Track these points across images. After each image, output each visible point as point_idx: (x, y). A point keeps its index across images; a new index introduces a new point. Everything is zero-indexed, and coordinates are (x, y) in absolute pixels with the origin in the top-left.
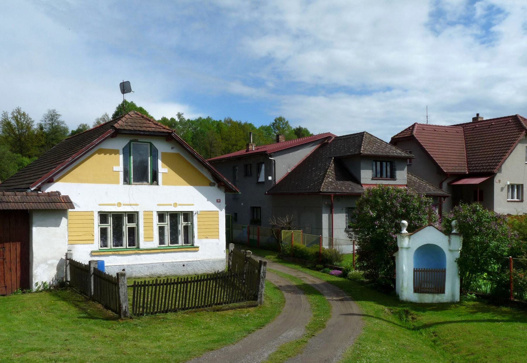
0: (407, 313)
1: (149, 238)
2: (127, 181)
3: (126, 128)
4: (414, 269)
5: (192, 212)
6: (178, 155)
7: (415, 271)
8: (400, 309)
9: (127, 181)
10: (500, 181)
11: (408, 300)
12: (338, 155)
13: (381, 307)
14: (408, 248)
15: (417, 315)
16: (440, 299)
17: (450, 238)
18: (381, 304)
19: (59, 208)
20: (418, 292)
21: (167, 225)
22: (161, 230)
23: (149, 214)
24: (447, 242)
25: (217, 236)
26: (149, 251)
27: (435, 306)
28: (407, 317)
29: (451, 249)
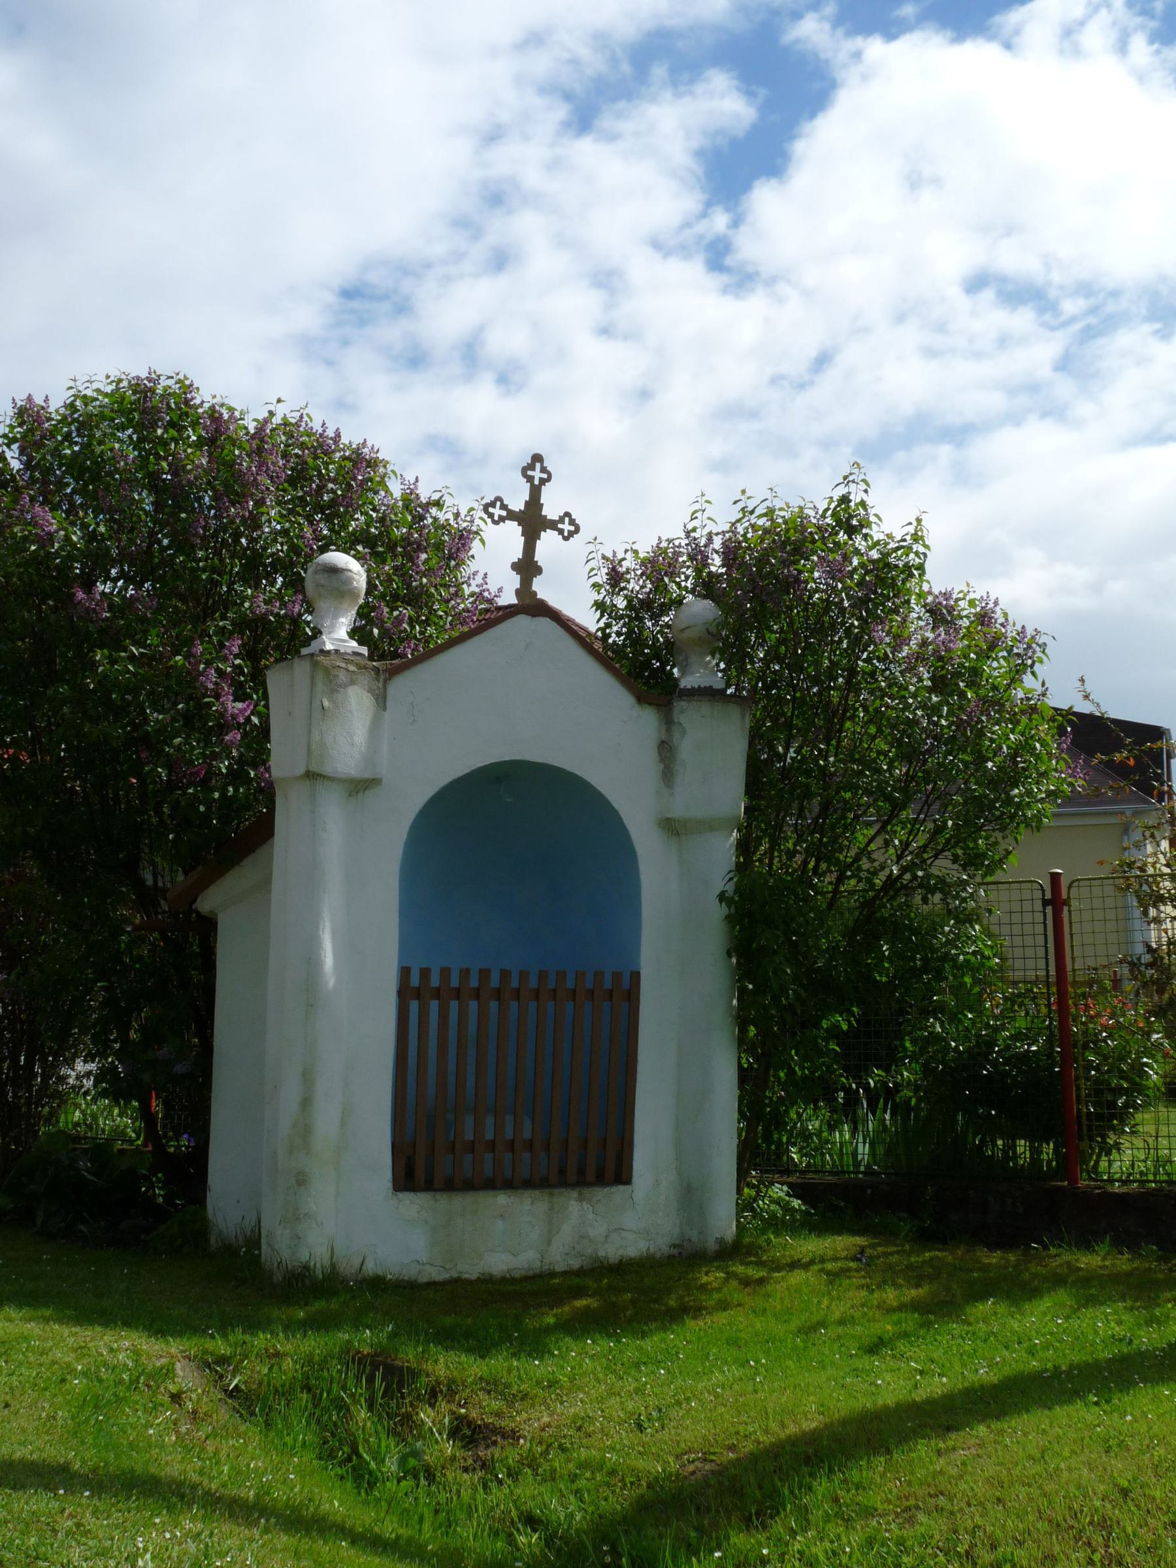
0: (391, 1381)
4: (405, 972)
7: (410, 992)
8: (312, 1344)
11: (348, 1266)
13: (122, 1347)
14: (360, 787)
15: (492, 1386)
16: (597, 1230)
17: (668, 721)
18: (106, 1318)
20: (429, 1186)
24: (648, 759)
27: (579, 1292)
28: (403, 1426)
29: (678, 811)
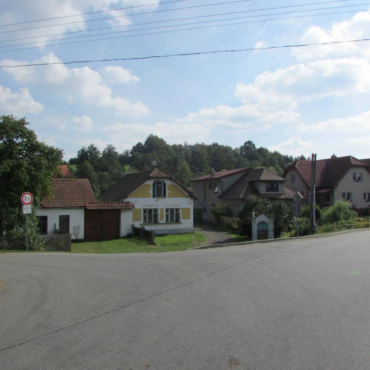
1: (162, 219)
2: (154, 197)
3: (154, 176)
5: (179, 208)
6: (174, 185)
9: (154, 197)
10: (337, 191)
12: (251, 180)
19: (129, 207)
21: (169, 213)
22: (167, 216)
23: (162, 210)
25: (189, 218)
26: (162, 224)
